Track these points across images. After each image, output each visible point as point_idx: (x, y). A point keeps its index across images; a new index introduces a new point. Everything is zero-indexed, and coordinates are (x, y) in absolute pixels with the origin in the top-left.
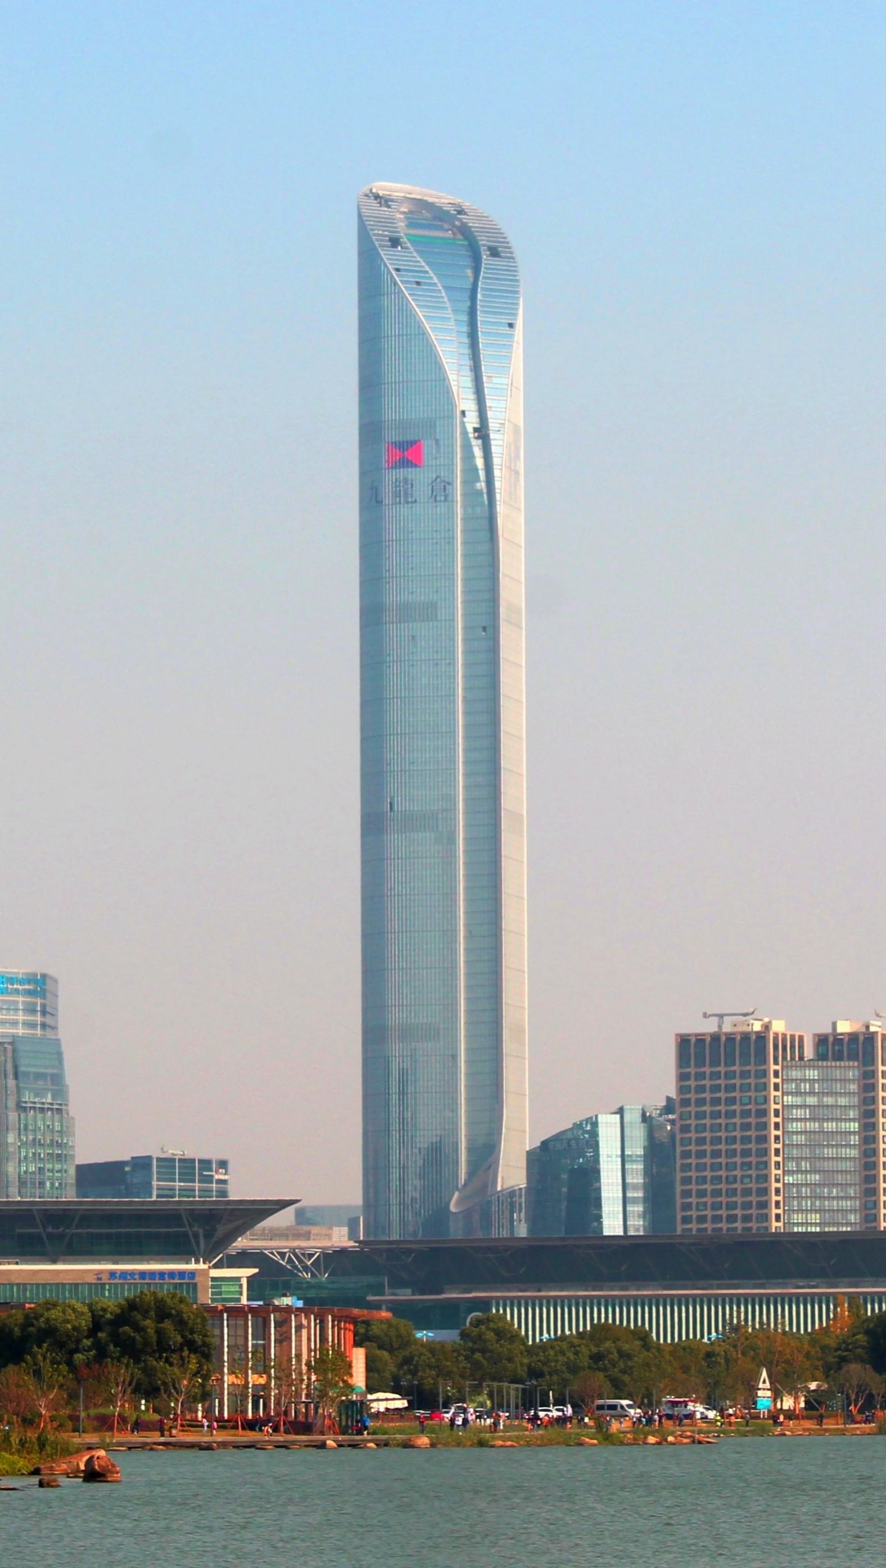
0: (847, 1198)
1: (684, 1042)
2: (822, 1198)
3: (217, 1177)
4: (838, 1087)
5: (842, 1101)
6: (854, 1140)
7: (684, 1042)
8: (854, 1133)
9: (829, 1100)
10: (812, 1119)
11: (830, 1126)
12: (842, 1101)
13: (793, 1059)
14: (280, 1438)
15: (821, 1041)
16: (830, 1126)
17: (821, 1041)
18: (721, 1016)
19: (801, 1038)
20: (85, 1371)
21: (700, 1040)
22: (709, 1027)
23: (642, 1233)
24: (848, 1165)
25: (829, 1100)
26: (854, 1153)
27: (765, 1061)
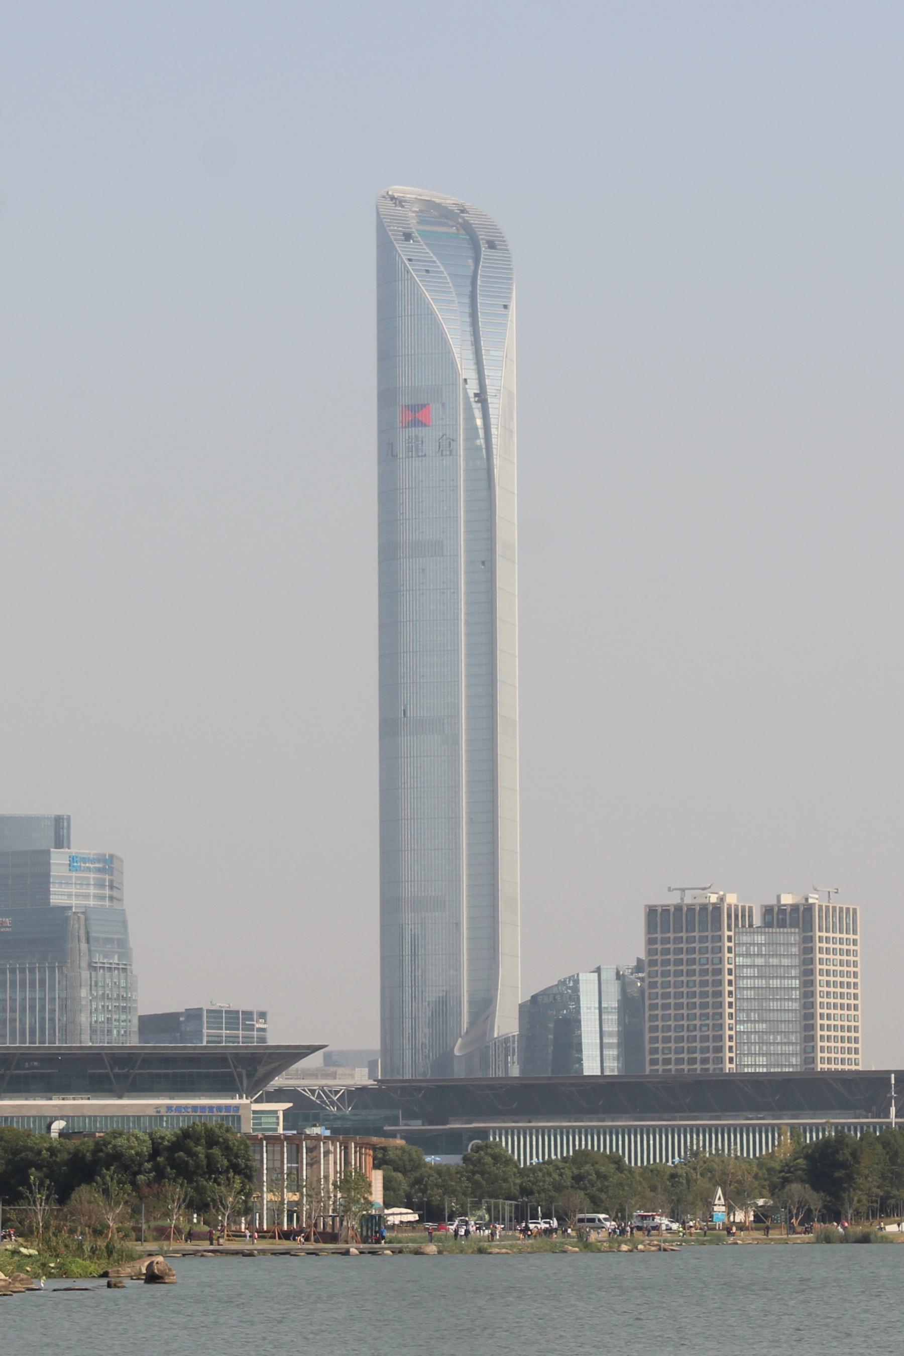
0: (789, 1043)
1: (651, 912)
3: (257, 1026)
5: (786, 962)
6: (796, 994)
7: (651, 912)
9: (774, 961)
12: (786, 962)
15: (768, 911)
17: (768, 911)
18: (683, 890)
19: (750, 909)
21: (665, 911)
22: (673, 899)
25: (774, 961)
27: (720, 928)
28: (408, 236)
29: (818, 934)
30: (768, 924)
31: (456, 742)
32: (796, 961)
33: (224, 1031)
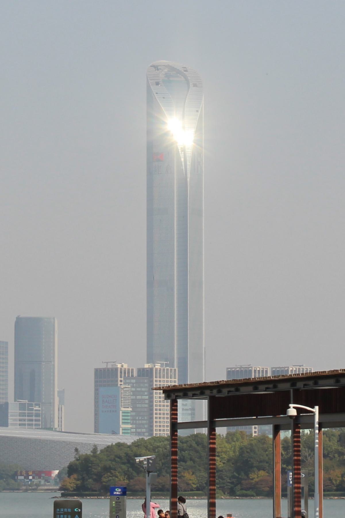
0: (144, 420)
1: (96, 370)
2: (136, 420)
3: (35, 409)
4: (142, 385)
5: (143, 389)
6: (147, 401)
7: (96, 370)
8: (147, 399)
9: (139, 389)
10: (133, 395)
11: (139, 397)
12: (143, 389)
13: (128, 376)
14: (289, 488)
15: (139, 370)
16: (139, 397)
17: (139, 370)
18: (107, 363)
19: (132, 370)
20: (24, 473)
21: (100, 370)
22: (104, 366)
23: (253, 426)
24: (146, 410)
25: (139, 389)
26: (146, 406)
27: (117, 377)
28: (157, 84)
29: (155, 379)
30: (139, 375)
31: (173, 289)
32: (147, 390)
33: (26, 412)
